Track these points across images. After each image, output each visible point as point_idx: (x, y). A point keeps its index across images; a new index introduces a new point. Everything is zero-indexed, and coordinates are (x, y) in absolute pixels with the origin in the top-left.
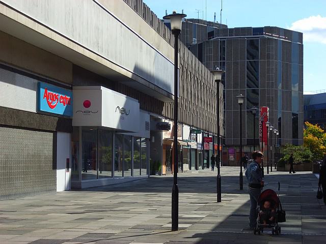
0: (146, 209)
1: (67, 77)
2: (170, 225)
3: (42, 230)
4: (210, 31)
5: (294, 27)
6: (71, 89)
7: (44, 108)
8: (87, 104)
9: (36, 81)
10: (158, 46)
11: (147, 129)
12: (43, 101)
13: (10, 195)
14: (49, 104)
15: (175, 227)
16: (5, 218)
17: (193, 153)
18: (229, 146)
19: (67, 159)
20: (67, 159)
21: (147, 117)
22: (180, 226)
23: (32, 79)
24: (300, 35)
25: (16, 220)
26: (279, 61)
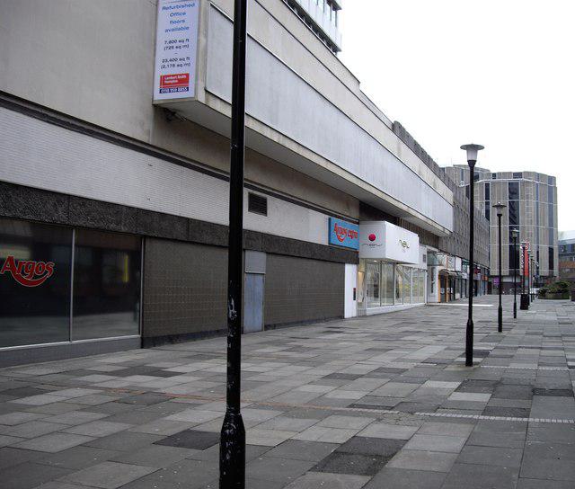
0: (431, 339)
1: (355, 214)
2: (464, 359)
3: (335, 362)
4: (268, 202)
5: (549, 173)
6: (358, 223)
7: (335, 241)
8: (372, 238)
9: (327, 216)
10: (435, 185)
11: (424, 261)
12: (334, 234)
13: (302, 322)
14: (339, 238)
15: (469, 363)
16: (300, 346)
17: (464, 282)
18: (492, 277)
19: (527, 309)
20: (527, 309)
21: (425, 249)
22: (474, 360)
23: (324, 215)
24: (552, 180)
25: (309, 349)
26: (533, 202)
